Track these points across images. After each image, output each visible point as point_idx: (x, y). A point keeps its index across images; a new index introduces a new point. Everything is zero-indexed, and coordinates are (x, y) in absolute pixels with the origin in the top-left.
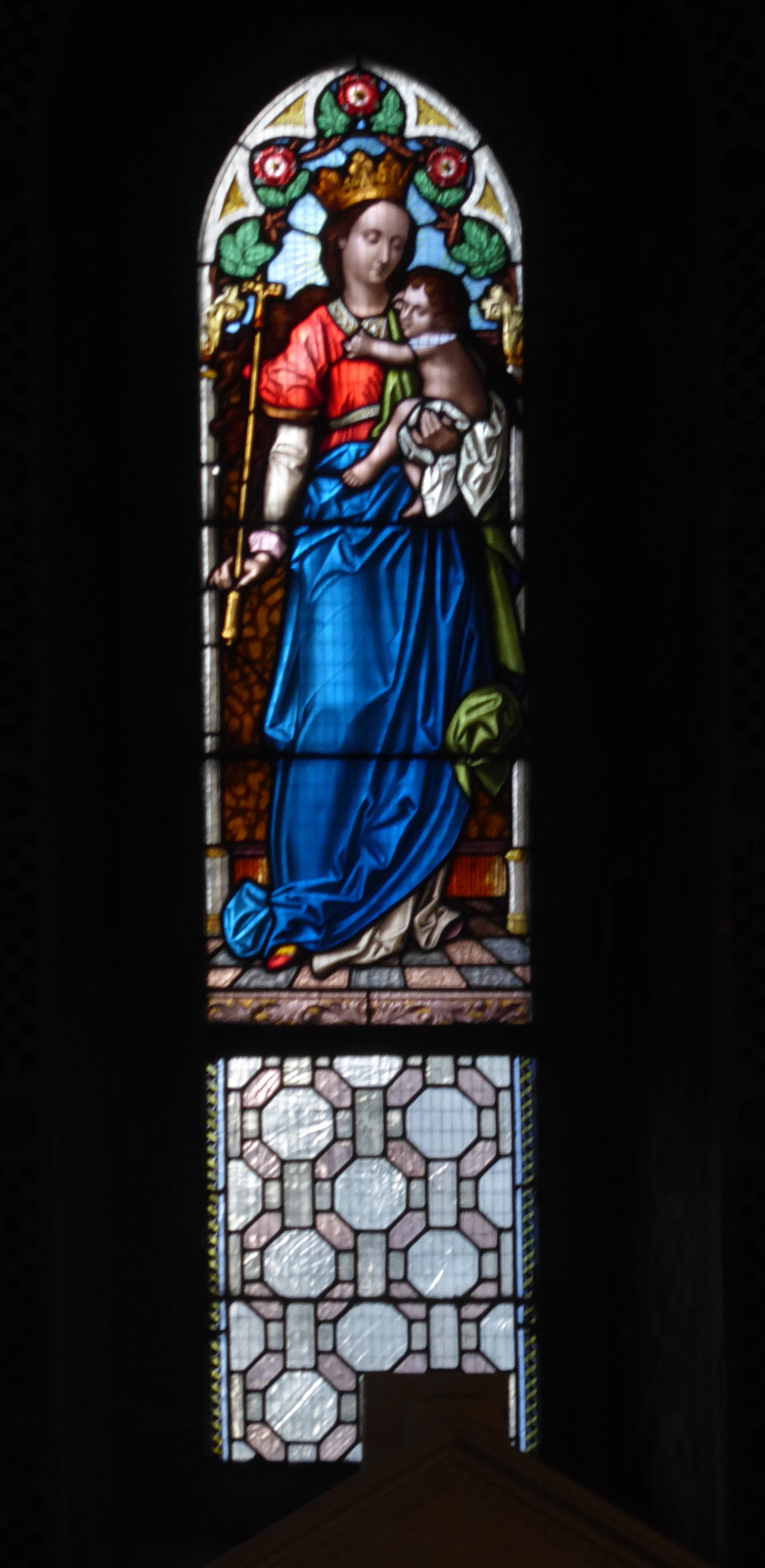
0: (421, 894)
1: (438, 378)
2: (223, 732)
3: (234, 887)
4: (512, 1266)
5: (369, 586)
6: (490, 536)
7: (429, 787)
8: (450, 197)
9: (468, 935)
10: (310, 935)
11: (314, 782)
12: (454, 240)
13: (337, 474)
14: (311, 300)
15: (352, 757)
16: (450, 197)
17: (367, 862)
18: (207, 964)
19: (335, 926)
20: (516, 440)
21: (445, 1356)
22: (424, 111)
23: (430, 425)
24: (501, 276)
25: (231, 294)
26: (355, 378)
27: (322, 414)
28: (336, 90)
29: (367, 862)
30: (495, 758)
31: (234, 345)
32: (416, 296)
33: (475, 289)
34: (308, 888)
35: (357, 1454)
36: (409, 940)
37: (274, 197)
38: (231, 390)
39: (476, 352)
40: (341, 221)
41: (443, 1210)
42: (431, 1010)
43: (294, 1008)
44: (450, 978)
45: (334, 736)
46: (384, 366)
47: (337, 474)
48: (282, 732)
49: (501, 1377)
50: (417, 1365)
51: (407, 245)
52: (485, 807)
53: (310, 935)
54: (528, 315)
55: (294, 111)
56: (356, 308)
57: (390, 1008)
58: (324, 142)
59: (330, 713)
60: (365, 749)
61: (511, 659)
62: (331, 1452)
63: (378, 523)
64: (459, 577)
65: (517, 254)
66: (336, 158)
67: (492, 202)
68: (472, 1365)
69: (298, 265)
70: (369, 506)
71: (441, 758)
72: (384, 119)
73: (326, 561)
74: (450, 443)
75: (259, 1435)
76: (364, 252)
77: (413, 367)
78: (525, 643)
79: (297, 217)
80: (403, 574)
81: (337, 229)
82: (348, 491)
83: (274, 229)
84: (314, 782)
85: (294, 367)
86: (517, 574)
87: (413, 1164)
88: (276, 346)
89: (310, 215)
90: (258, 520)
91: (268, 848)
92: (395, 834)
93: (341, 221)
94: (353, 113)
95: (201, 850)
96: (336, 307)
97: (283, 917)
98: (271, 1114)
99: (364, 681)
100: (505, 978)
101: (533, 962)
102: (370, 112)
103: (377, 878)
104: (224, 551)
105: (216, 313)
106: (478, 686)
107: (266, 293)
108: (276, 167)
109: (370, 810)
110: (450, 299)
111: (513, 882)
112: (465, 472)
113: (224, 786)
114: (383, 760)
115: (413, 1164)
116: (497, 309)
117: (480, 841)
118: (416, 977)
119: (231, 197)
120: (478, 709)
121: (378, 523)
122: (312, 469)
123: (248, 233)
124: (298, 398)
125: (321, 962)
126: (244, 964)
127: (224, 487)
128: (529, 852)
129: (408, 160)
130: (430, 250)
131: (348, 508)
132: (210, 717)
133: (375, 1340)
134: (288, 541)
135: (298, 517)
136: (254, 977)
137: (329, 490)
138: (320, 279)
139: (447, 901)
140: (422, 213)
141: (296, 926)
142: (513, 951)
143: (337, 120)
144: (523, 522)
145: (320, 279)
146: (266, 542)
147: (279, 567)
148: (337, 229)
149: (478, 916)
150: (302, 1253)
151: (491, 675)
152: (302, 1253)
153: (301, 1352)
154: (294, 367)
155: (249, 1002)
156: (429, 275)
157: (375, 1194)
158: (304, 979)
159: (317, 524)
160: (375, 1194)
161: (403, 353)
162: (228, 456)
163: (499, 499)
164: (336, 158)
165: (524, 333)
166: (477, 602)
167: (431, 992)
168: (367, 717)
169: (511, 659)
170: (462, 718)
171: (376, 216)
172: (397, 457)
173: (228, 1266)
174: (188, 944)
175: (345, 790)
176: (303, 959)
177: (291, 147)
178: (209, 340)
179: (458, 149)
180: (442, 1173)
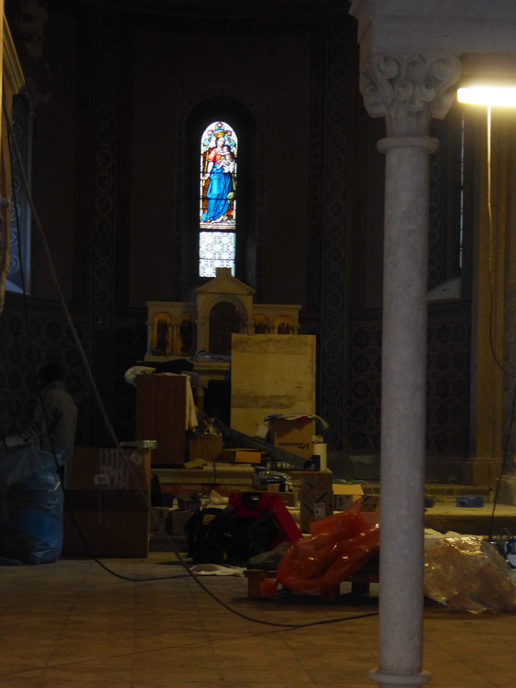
0: (224, 214)
1: (228, 157)
2: (203, 196)
3: (203, 213)
4: (233, 256)
5: (219, 180)
6: (233, 175)
7: (225, 202)
8: (229, 137)
9: (229, 219)
10: (211, 219)
11: (212, 202)
12: (230, 142)
13: (216, 167)
14: (214, 148)
15: (217, 199)
16: (229, 137)
17: (218, 211)
18: (200, 222)
19: (214, 218)
20: (236, 164)
21: (225, 266)
22: (226, 127)
23: (227, 163)
24: (235, 146)
25: (205, 147)
26: (218, 157)
27: (215, 160)
28: (217, 124)
29: (218, 211)
30: (233, 200)
31: (205, 153)
32: (225, 148)
33: (232, 147)
34: (211, 214)
35: (215, 276)
36: (222, 220)
37: (210, 136)
38: (205, 158)
39: (232, 154)
40: (217, 139)
41: (225, 250)
42: (224, 228)
43: (209, 227)
44: (227, 224)
45: (215, 197)
46: (222, 156)
47: (216, 167)
48: (209, 196)
49: (231, 268)
50: (222, 267)
51: (224, 142)
52: (231, 205)
53: (211, 219)
54: (238, 150)
55: (213, 126)
56: (218, 149)
57: (220, 227)
58: (216, 130)
59: (214, 194)
60: (218, 199)
61: (235, 189)
62: (212, 276)
63: (220, 173)
64: (229, 180)
65: (237, 143)
66: (217, 132)
67: (234, 138)
68: (228, 267)
69: (212, 144)
70: (219, 171)
71: (227, 200)
72: (222, 128)
73: (214, 177)
74: (228, 165)
75: (204, 274)
76: (220, 143)
77: (225, 156)
78: (236, 187)
79: (212, 139)
80: (223, 179)
81: (218, 142)
82: (217, 170)
83: (210, 140)
84: (212, 202)
85: (211, 156)
86: (236, 179)
87: (222, 245)
88: (209, 153)
89: (214, 139)
90: (207, 173)
91: (207, 209)
92: (221, 208)
93: (217, 139)
94: (219, 127)
95: (200, 209)
96: (216, 149)
97: (209, 217)
98: (205, 239)
99: (218, 191)
100: (233, 224)
101: (236, 223)
102: (221, 127)
103: (219, 213)
104: (203, 176)
105: (203, 149)
106: (231, 192)
107: (250, 322)
108: (210, 133)
109: (218, 205)
110: (229, 148)
111: (234, 214)
112: (231, 167)
113: (203, 202)
114: (220, 200)
115: (222, 245)
116: (234, 150)
117: (230, 209)
118: (223, 224)
119: (205, 136)
120: (231, 195)
121: (220, 173)
122: (214, 167)
123: (207, 140)
124: (212, 159)
125: (213, 222)
126: (204, 222)
127: (204, 169)
128: (237, 211)
129: (225, 133)
130: (227, 143)
131: (217, 171)
132: (201, 194)
133: (218, 264)
134: (211, 175)
135: (211, 172)
136: (205, 223)
137: (215, 169)
138: (215, 146)
139: (227, 216)
140: (226, 139)
141: (210, 218)
142: (234, 221)
143: (217, 128)
144: (237, 173)
145: (215, 146)
146: (208, 175)
147: (209, 178)
148: (218, 142)
149: (230, 217)
150: (41, 543)
151: (232, 190)
152: (41, 543)
153: (209, 265)
154: (211, 156)
155: (205, 226)
156: (227, 145)
157: (218, 248)
158: (211, 224)
159: (214, 173)
160: (218, 248)
161: (223, 154)
162: (204, 165)
163: (234, 171)
164: (217, 132)
165: (238, 152)
166: (231, 182)
167: (224, 226)
168: (219, 195)
169: (235, 189)
170: (229, 195)
171: (222, 139)
172: (223, 166)
173: (201, 255)
174: (198, 220)
175: (216, 203)
176: (210, 222)
177: (212, 131)
178: (202, 152)
179: (230, 132)
180: (225, 246)
